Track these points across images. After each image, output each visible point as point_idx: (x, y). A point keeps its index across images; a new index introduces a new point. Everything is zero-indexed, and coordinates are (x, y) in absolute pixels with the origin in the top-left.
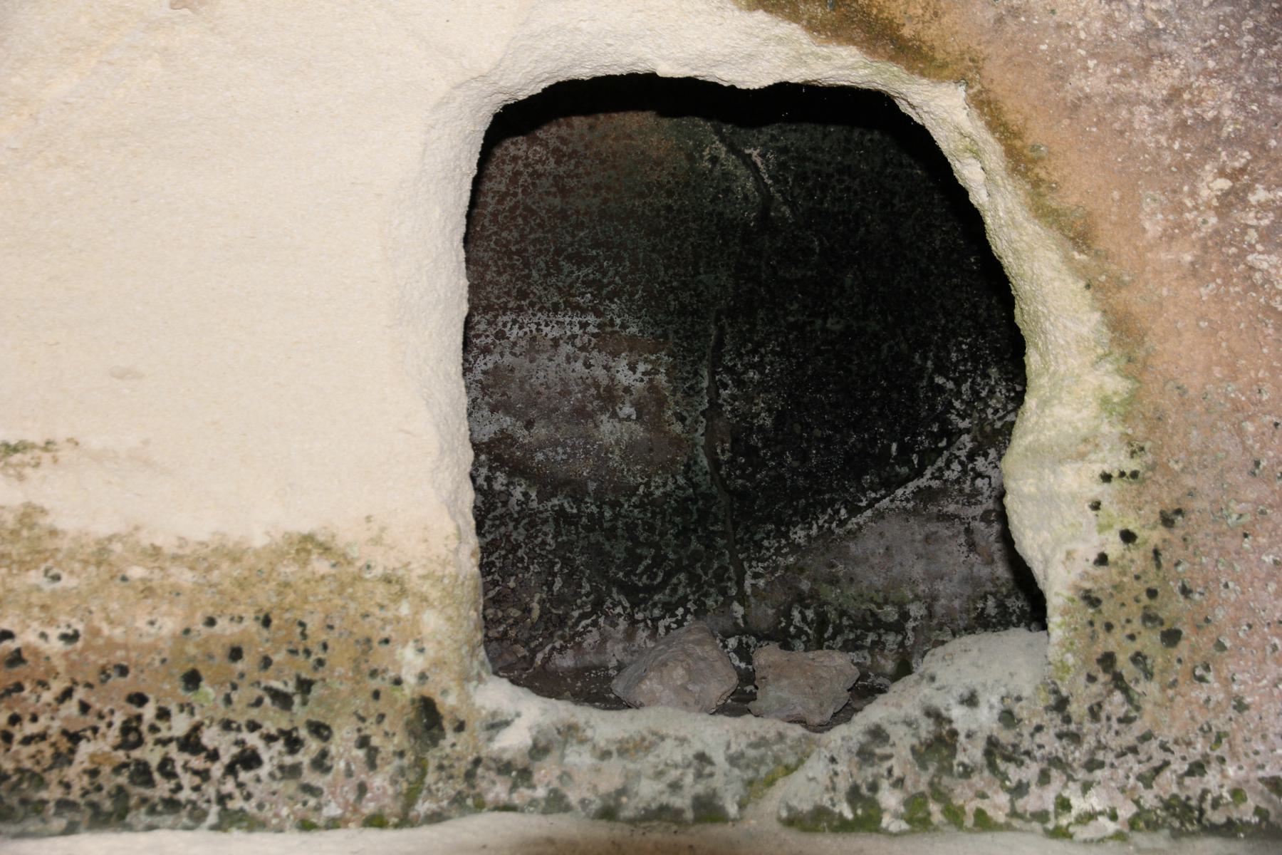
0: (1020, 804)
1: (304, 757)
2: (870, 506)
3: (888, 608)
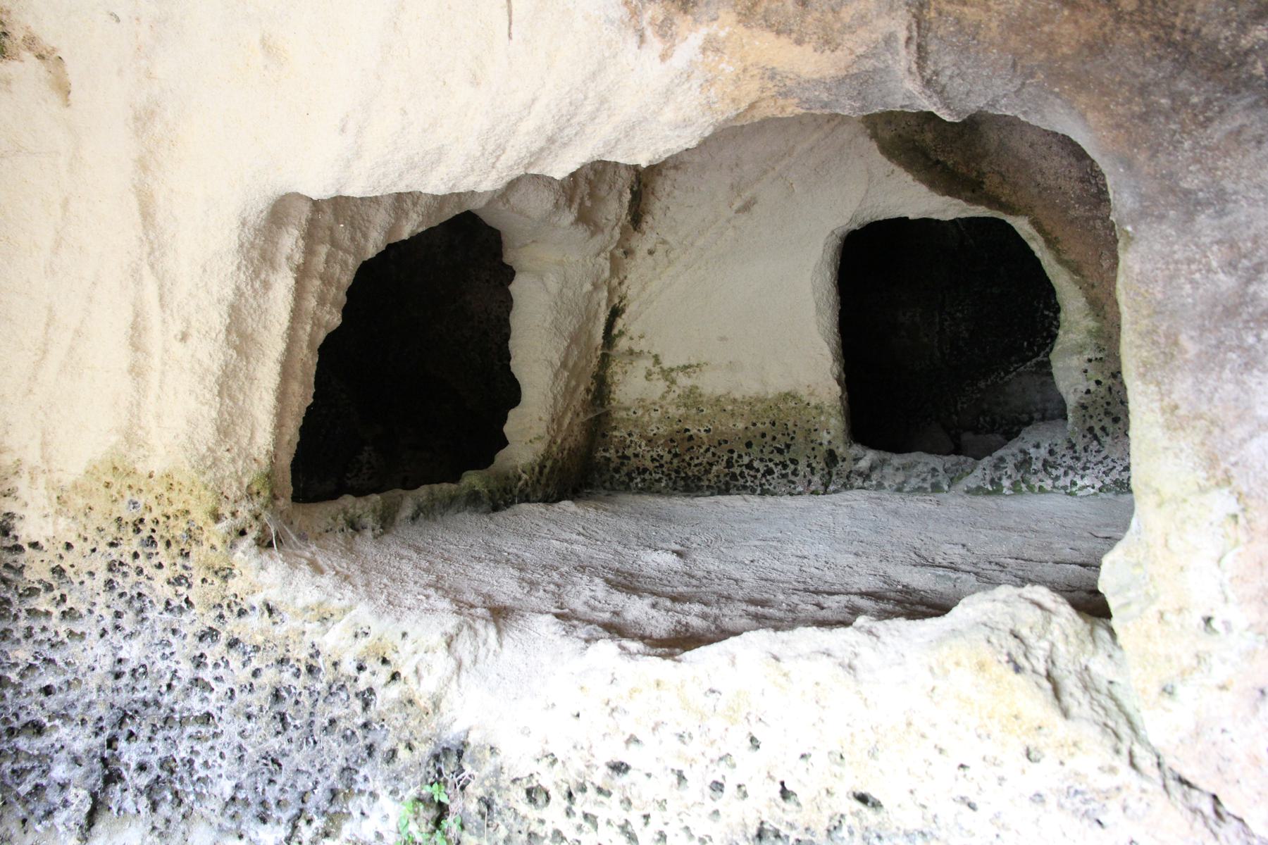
0: (1057, 484)
1: (789, 471)
2: (1015, 370)
3: (1024, 415)
